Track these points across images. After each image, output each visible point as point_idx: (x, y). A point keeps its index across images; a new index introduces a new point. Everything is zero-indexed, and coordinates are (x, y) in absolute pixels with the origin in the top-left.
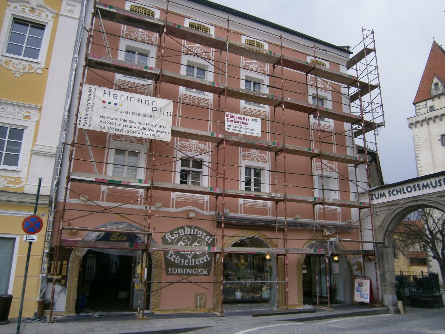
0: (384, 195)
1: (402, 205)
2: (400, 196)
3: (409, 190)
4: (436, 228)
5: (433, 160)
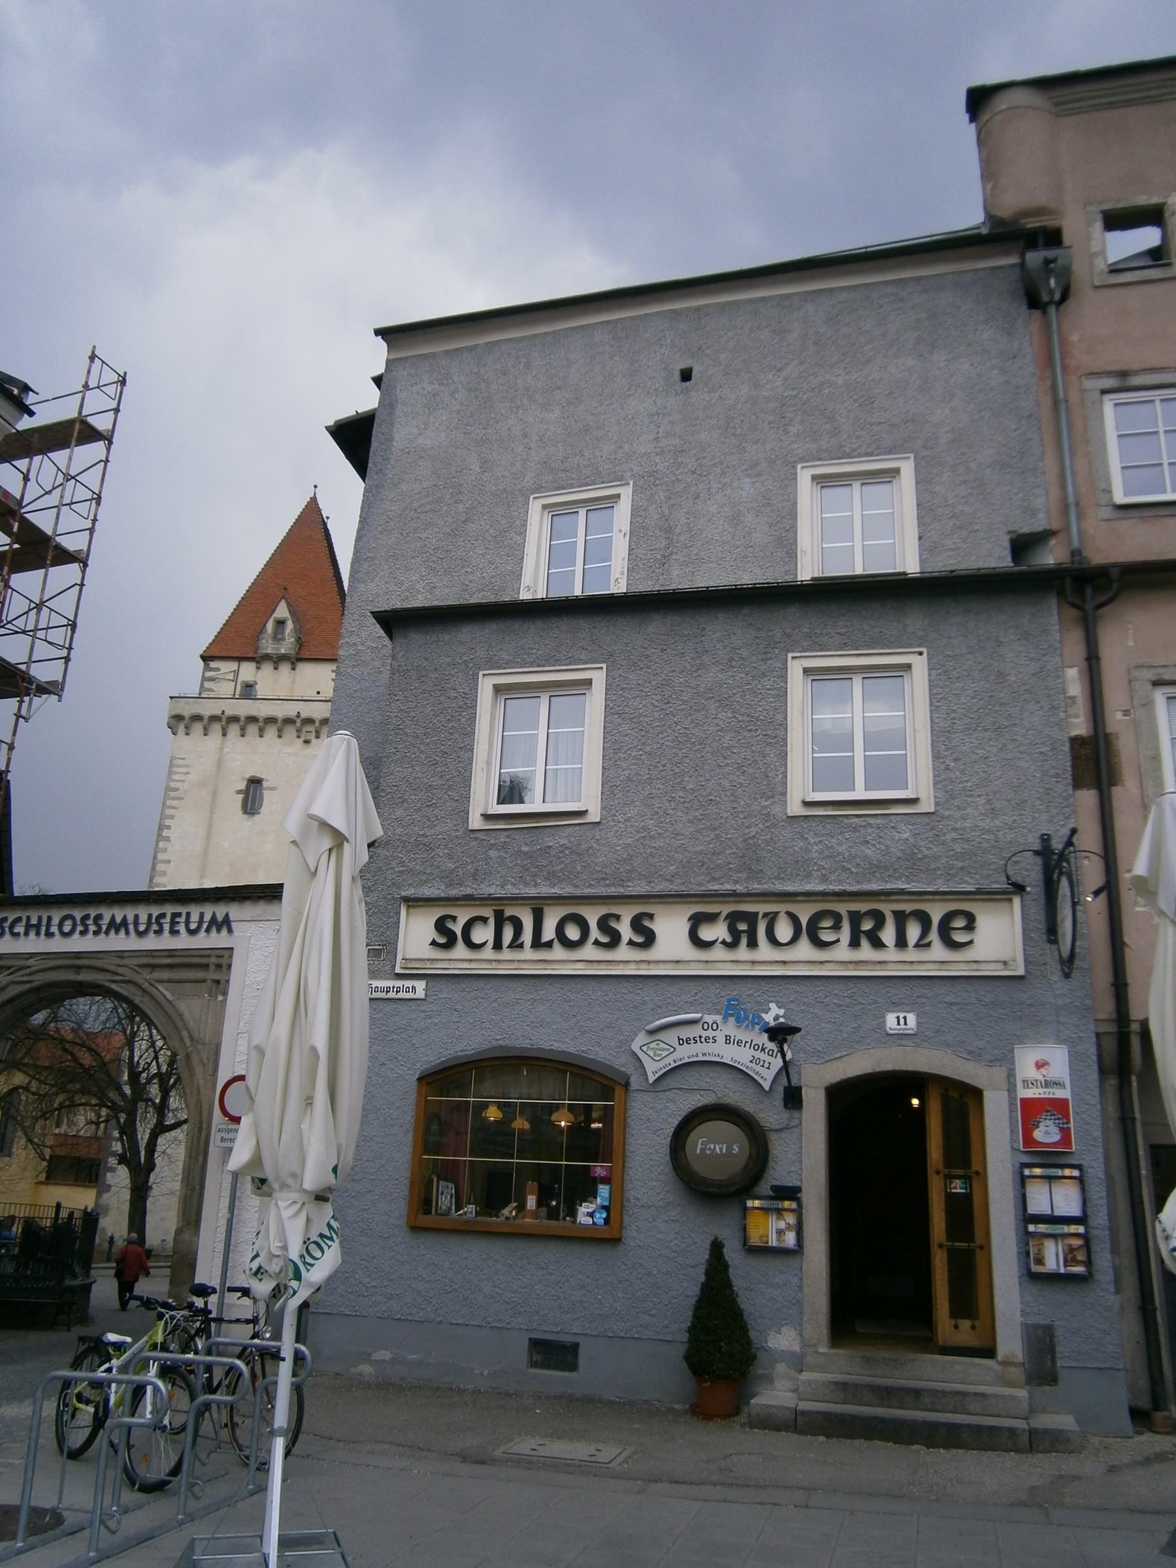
1: (31, 974)
2: (32, 944)
3: (67, 928)
4: (154, 1063)
5: (206, 851)
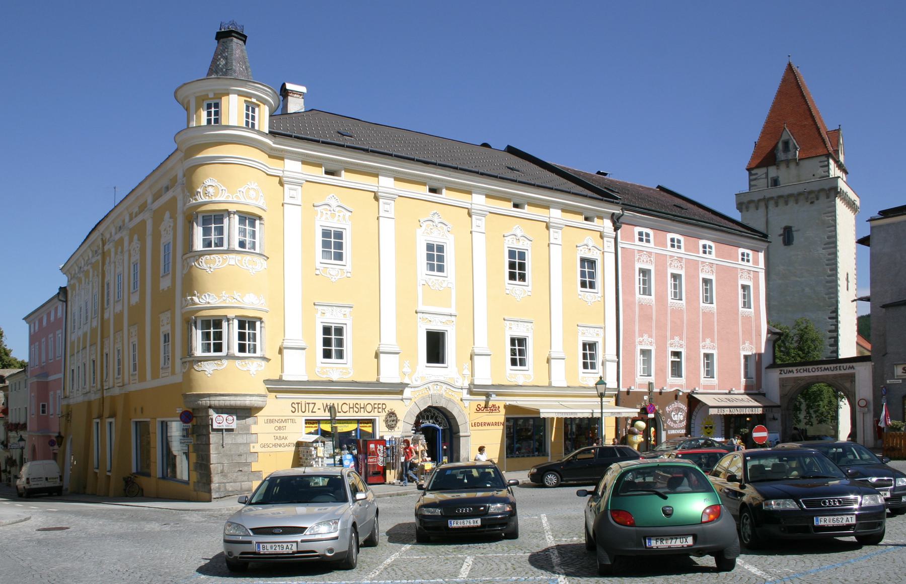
0: (792, 371)
